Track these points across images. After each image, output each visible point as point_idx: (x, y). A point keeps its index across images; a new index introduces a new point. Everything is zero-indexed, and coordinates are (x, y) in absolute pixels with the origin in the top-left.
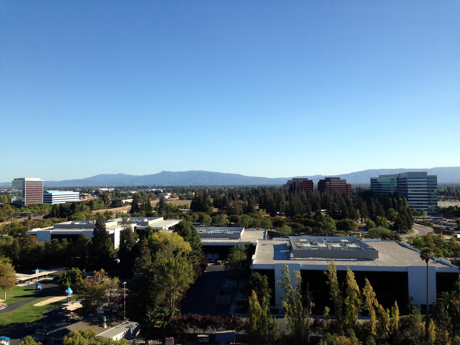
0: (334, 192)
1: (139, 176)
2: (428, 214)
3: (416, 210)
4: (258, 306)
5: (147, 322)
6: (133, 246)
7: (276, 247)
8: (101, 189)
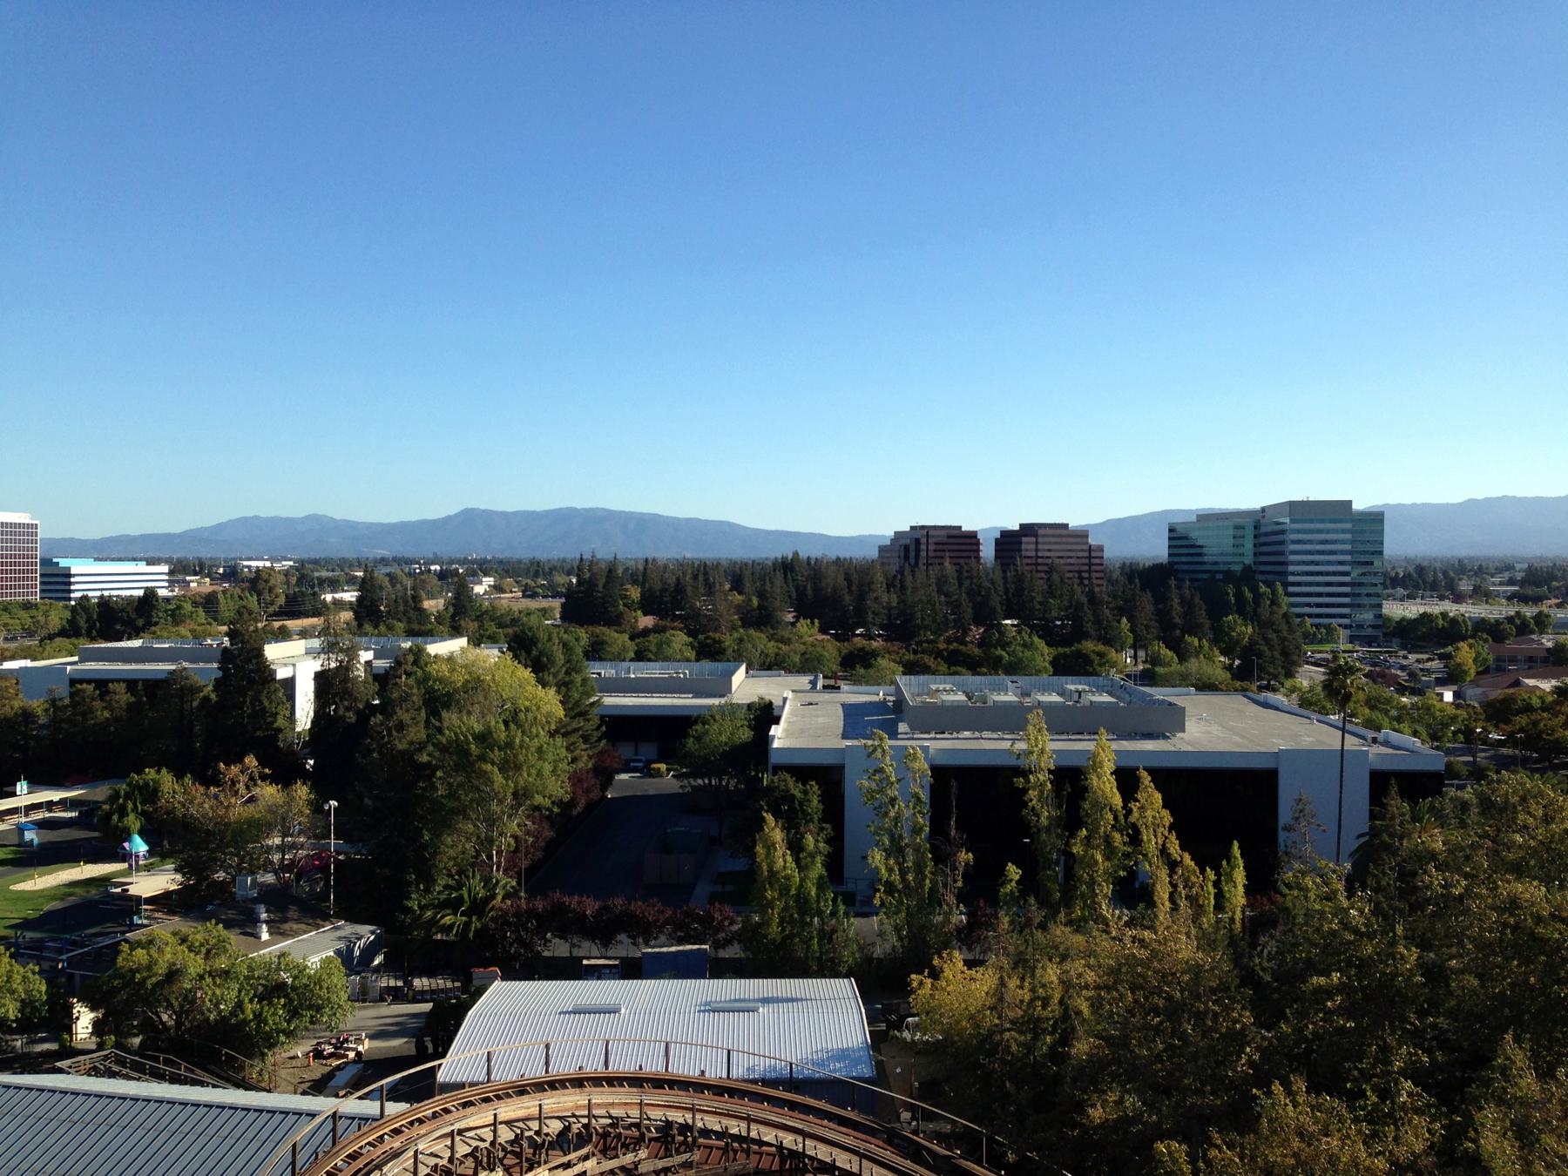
2: (1352, 639)
8: (245, 563)
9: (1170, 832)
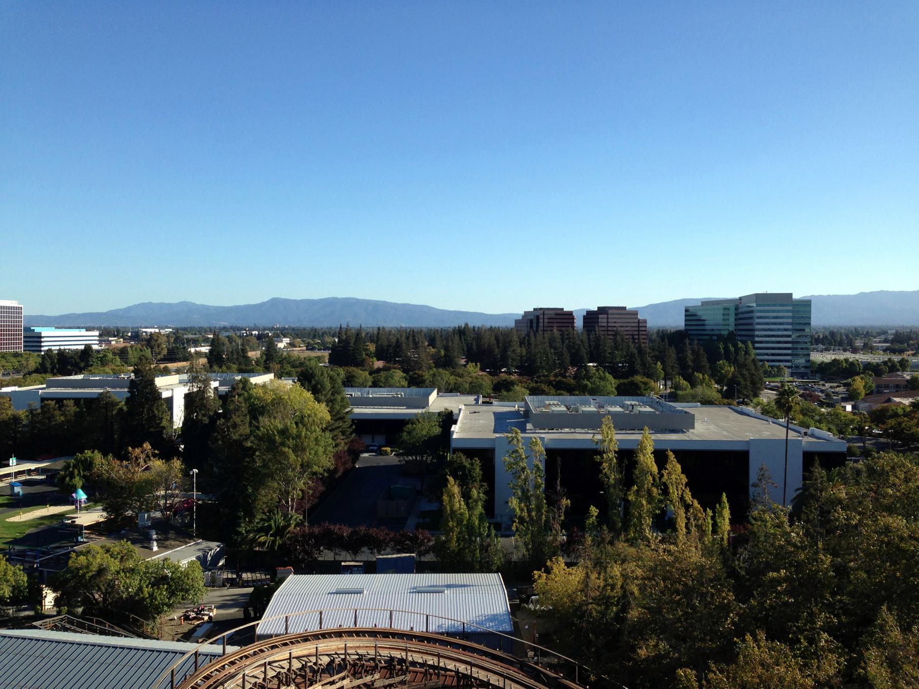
2: (792, 375)
8: (144, 330)
9: (686, 487)
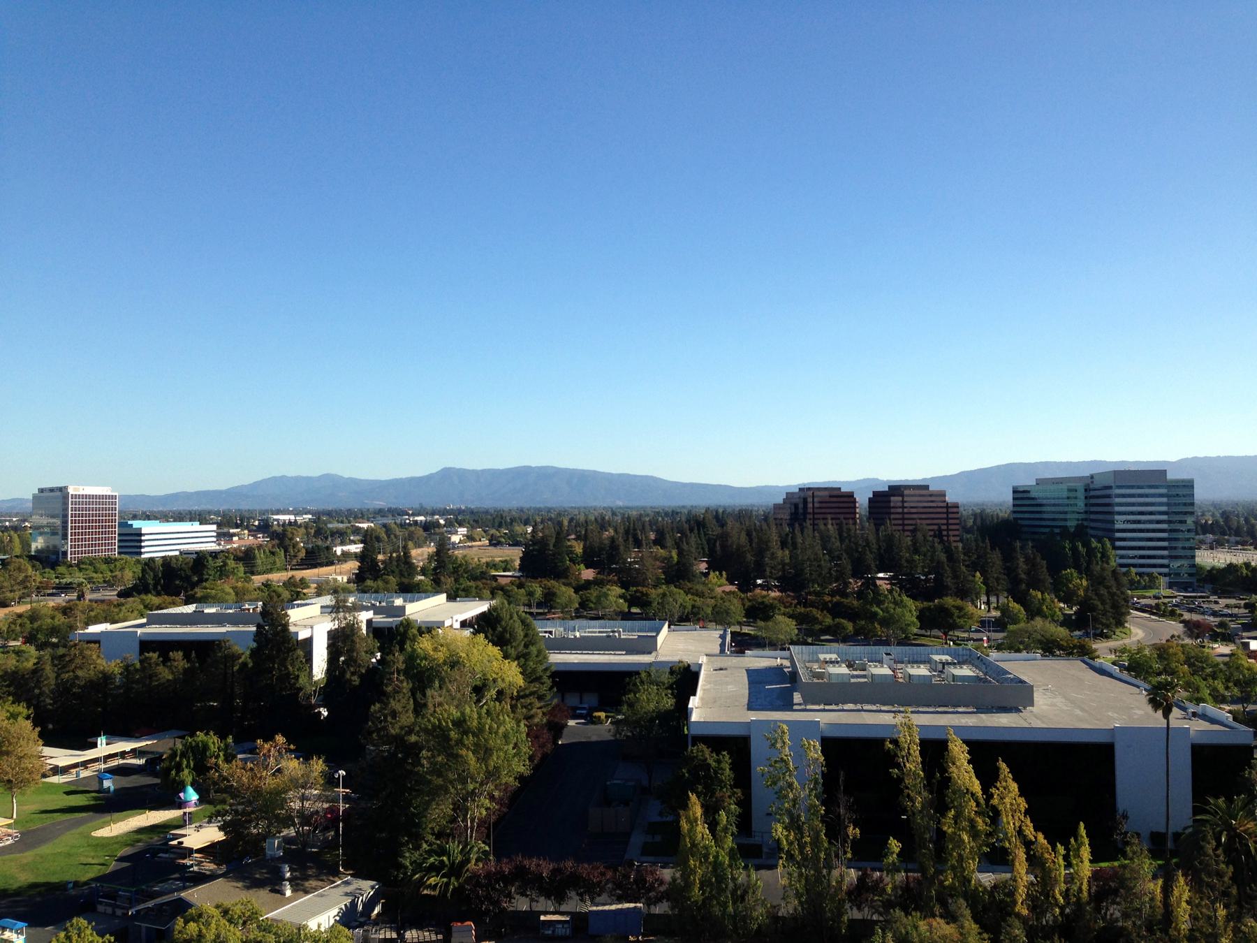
0: (911, 525)
1: (381, 481)
2: (1171, 586)
3: (1136, 574)
4: (705, 836)
5: (402, 879)
6: (364, 671)
7: (753, 675)
8: (275, 517)
